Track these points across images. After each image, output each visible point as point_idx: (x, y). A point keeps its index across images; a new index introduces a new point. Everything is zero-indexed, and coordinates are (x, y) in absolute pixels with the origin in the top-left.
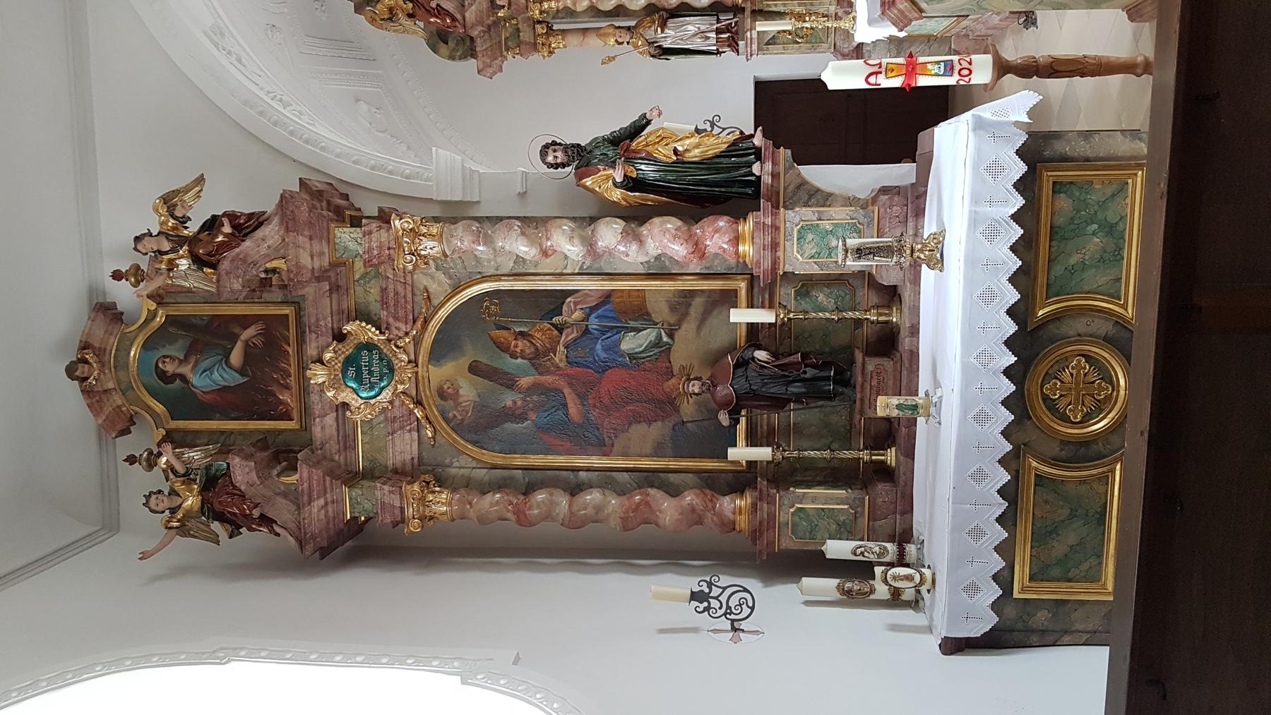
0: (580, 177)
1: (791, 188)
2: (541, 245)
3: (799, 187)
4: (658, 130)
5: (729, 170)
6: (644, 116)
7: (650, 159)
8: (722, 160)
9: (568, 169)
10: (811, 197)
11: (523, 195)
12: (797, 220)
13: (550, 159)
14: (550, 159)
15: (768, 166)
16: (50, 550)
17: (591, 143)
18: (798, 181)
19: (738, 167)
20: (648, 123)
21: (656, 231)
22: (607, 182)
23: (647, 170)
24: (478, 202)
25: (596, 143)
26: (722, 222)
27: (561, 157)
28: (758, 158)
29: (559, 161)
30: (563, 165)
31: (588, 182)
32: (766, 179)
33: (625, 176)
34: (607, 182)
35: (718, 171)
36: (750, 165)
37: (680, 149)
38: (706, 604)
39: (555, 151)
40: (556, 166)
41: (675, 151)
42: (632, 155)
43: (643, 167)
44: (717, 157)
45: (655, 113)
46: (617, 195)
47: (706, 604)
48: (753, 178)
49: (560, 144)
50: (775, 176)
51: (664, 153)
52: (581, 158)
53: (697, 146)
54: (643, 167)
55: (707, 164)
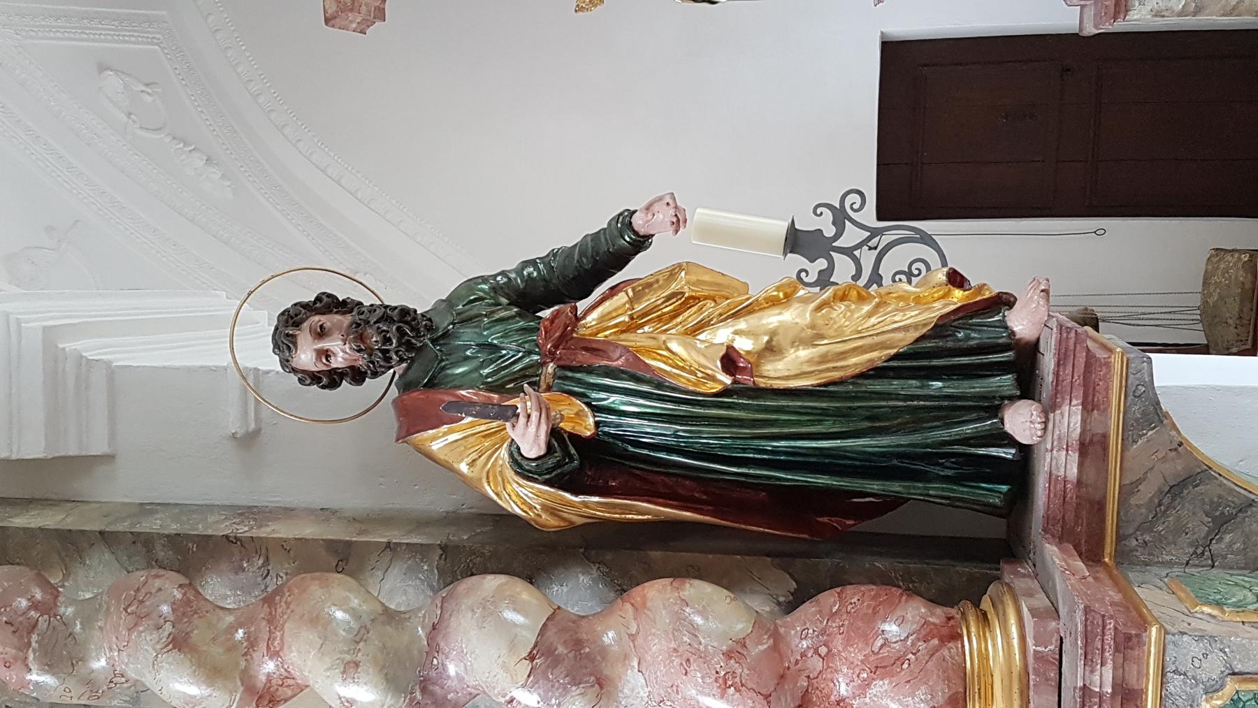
0: (414, 420)
1: (1147, 492)
2: (247, 678)
3: (1176, 489)
4: (673, 273)
5: (920, 417)
6: (625, 220)
7: (637, 375)
8: (895, 385)
9: (374, 387)
10: (1220, 523)
11: (248, 440)
12: (1213, 667)
13: (305, 357)
14: (305, 357)
15: (1070, 419)
16: (269, 276)
17: (450, 302)
18: (1177, 467)
19: (951, 410)
20: (641, 243)
21: (657, 646)
22: (491, 456)
23: (633, 417)
24: (108, 458)
25: (469, 303)
26: (901, 624)
27: (342, 354)
28: (1027, 388)
29: (338, 362)
30: (357, 376)
31: (439, 441)
32: (1058, 465)
33: (555, 433)
34: (491, 456)
35: (877, 424)
36: (993, 407)
37: (744, 345)
38: (822, 264)
39: (321, 333)
40: (332, 379)
41: (730, 361)
42: (584, 358)
43: (613, 400)
44: (877, 373)
45: (664, 215)
46: (524, 498)
47: (822, 264)
48: (1008, 453)
49: (343, 306)
50: (1091, 447)
51: (690, 357)
52: (406, 350)
53: (813, 337)
54: (613, 400)
55: (835, 399)
